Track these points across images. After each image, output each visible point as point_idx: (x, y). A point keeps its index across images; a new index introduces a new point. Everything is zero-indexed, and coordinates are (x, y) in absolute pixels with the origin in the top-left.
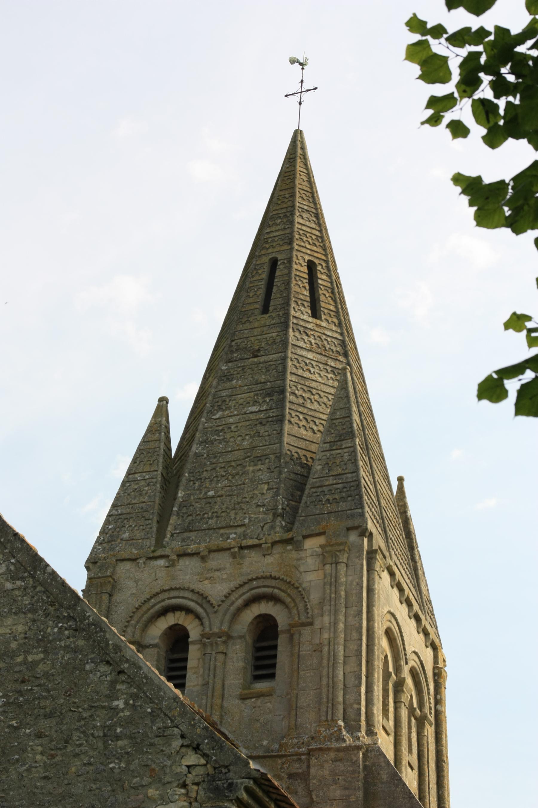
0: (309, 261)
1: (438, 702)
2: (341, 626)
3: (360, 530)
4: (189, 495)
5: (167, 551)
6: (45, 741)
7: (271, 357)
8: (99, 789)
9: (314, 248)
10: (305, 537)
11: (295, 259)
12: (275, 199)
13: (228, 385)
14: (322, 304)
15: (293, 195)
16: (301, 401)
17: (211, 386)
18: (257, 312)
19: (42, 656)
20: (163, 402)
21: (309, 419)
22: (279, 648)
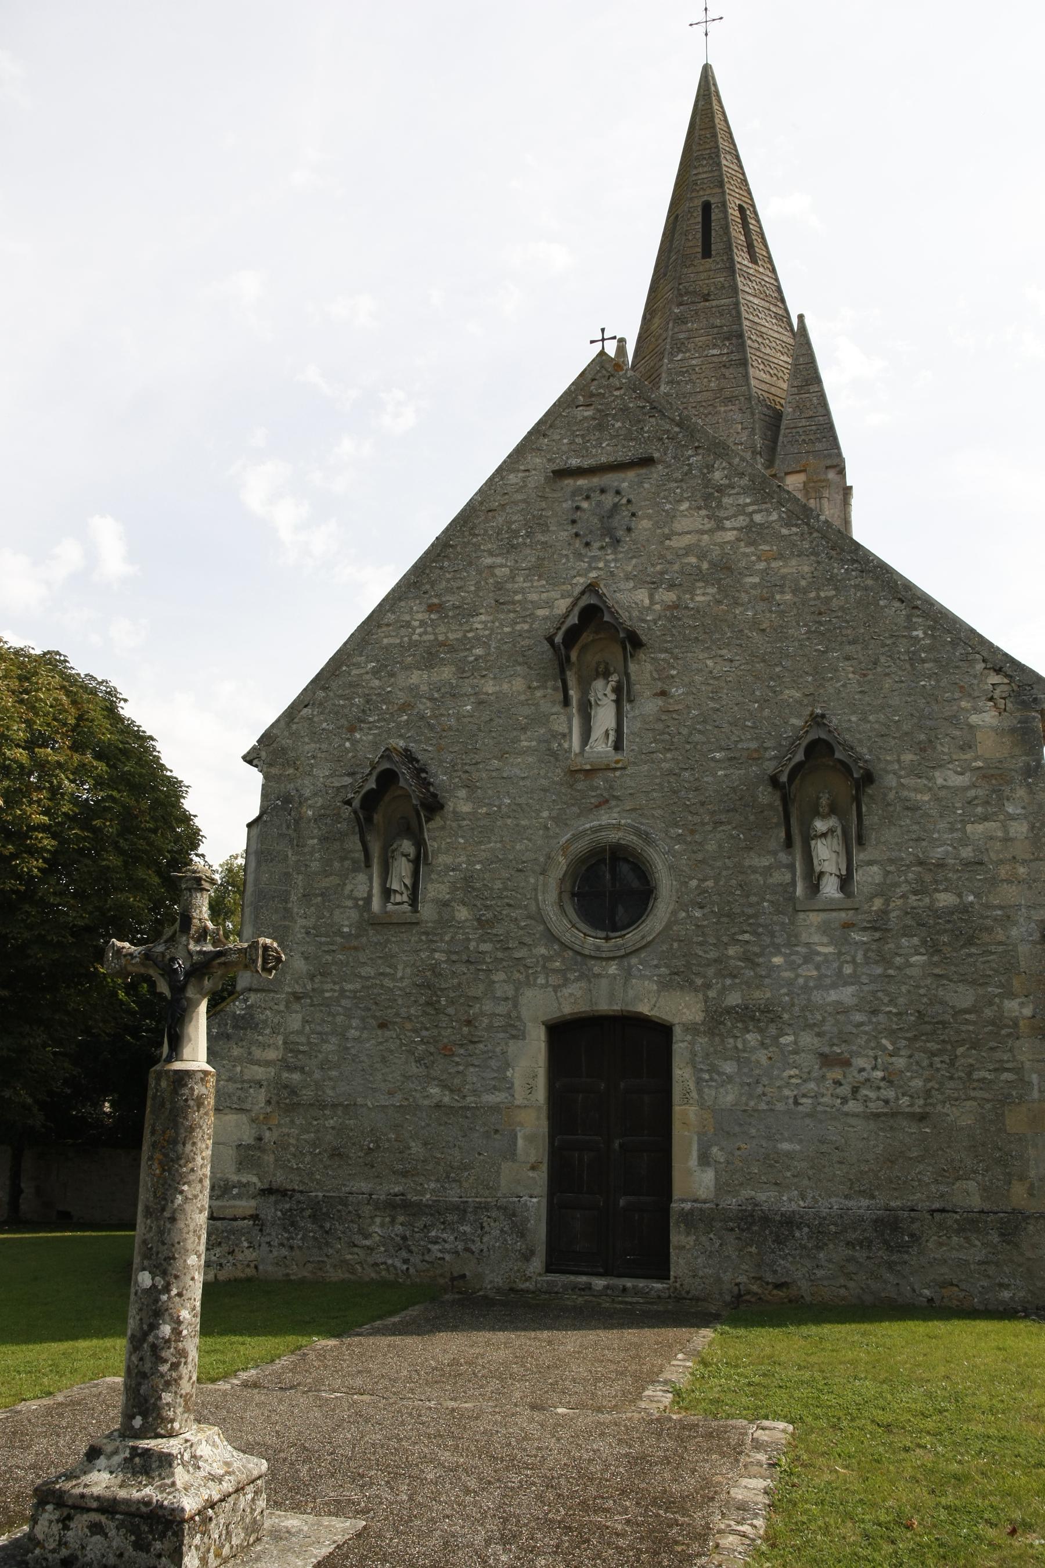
3: (838, 469)
6: (854, 662)
7: (723, 302)
10: (787, 474)
13: (684, 328)
18: (699, 255)
19: (834, 593)
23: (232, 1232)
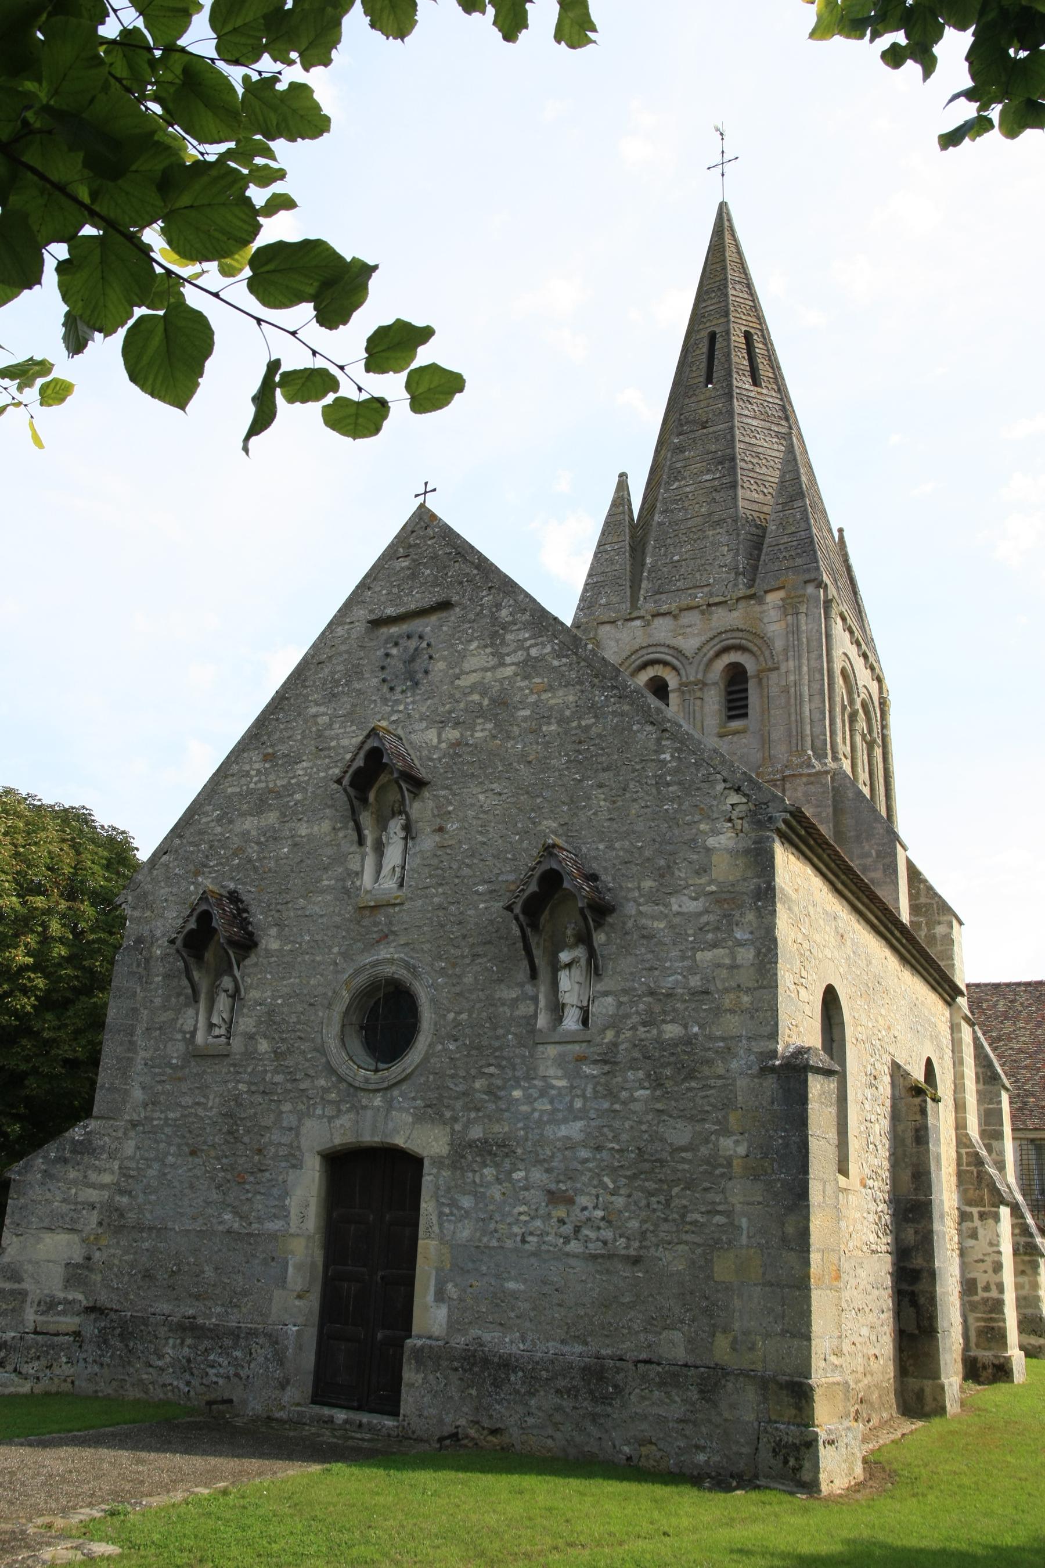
0: (746, 331)
1: (884, 727)
2: (805, 669)
3: (816, 582)
4: (657, 561)
5: (642, 613)
6: (606, 790)
7: (719, 427)
8: (658, 826)
9: (749, 318)
10: (766, 592)
11: (732, 331)
12: (707, 274)
13: (681, 457)
14: (761, 372)
15: (724, 268)
16: (751, 466)
17: (665, 458)
19: (593, 720)
20: (623, 476)
21: (759, 482)
22: (750, 691)
23: (52, 1347)
